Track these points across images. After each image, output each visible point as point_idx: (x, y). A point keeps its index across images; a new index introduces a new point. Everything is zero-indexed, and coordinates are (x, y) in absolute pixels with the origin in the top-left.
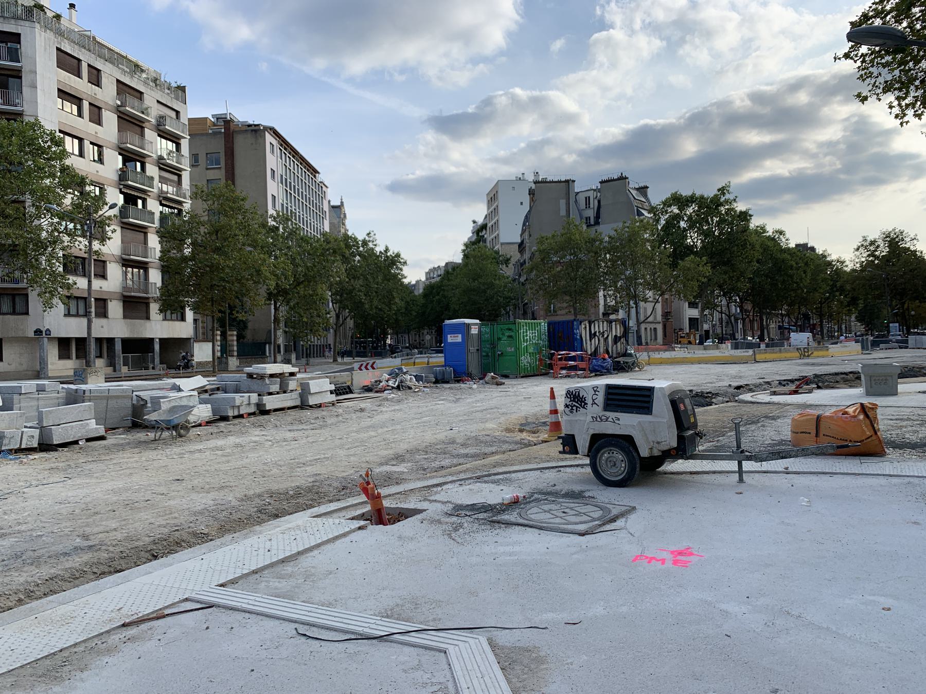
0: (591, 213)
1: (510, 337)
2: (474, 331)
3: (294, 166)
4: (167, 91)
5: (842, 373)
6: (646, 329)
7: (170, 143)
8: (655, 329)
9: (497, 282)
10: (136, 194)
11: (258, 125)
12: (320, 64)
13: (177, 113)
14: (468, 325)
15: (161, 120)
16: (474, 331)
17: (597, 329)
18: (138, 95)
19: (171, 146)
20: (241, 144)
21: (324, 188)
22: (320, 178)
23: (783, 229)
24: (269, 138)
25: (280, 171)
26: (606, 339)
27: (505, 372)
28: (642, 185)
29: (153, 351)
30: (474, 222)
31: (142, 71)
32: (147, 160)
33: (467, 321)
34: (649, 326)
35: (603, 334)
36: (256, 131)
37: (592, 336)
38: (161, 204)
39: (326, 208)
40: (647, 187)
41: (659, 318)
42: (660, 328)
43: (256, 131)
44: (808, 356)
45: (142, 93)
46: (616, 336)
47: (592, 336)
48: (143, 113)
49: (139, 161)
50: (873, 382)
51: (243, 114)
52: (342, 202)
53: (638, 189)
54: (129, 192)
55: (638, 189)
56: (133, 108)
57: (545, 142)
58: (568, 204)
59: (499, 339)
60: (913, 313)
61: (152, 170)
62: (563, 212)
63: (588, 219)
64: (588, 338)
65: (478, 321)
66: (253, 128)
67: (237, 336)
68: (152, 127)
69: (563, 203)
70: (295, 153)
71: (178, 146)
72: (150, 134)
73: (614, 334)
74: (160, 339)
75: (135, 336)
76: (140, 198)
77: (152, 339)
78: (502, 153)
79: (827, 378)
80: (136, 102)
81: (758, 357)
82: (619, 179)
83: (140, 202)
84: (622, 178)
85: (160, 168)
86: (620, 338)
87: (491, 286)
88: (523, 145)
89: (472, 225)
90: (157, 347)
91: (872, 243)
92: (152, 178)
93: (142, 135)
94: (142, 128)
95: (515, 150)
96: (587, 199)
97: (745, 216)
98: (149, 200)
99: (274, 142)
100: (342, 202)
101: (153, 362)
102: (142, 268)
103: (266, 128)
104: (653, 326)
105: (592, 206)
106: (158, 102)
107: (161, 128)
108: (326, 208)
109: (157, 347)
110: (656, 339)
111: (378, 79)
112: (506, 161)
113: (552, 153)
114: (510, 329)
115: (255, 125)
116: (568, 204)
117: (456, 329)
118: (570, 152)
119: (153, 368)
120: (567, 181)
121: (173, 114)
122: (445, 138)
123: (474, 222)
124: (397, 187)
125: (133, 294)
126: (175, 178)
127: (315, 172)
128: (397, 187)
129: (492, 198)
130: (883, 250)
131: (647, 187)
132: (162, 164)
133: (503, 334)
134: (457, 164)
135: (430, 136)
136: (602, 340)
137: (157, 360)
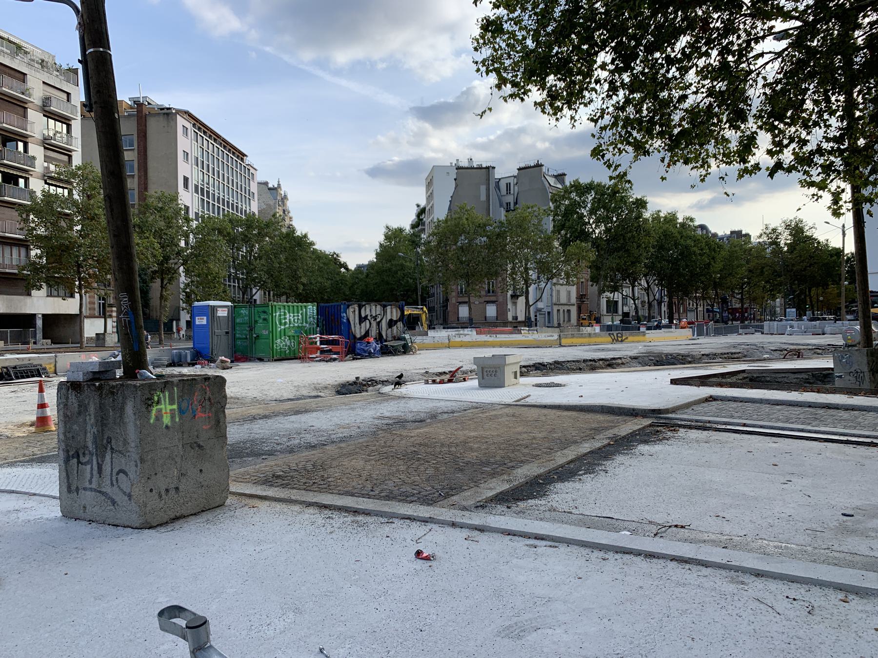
0: (510, 199)
1: (265, 319)
2: (222, 313)
3: (211, 147)
4: (55, 73)
5: (590, 360)
6: (558, 310)
7: (59, 124)
8: (569, 311)
9: (408, 264)
10: (18, 173)
11: (170, 109)
12: (307, 55)
13: (68, 94)
14: (214, 309)
15: (47, 101)
16: (222, 313)
17: (368, 312)
18: (22, 76)
19: (62, 128)
20: (153, 126)
21: (252, 171)
22: (247, 160)
23: (693, 217)
24: (181, 121)
25: (195, 152)
26: (379, 323)
27: (260, 355)
28: (560, 172)
29: (34, 326)
30: (418, 206)
31: (26, 53)
32: (29, 140)
33: (212, 303)
34: (561, 308)
35: (375, 318)
36: (168, 114)
37: (362, 320)
38: (46, 183)
39: (254, 188)
40: (565, 175)
41: (574, 300)
42: (574, 310)
43: (168, 114)
44: (622, 341)
45: (25, 74)
46: (391, 320)
47: (362, 320)
48: (23, 94)
49: (21, 141)
50: (485, 374)
51: (160, 99)
52: (279, 185)
53: (556, 177)
54: (6, 170)
55: (556, 177)
56: (11, 89)
57: (522, 131)
58: (488, 190)
59: (256, 322)
60: (821, 298)
61: (36, 150)
62: (483, 198)
63: (508, 204)
64: (357, 321)
65: (229, 304)
66: (165, 111)
67: (117, 312)
68: (36, 108)
69: (483, 188)
70: (215, 137)
71: (69, 127)
72: (34, 116)
73: (389, 318)
74: (43, 315)
75: (12, 312)
76: (22, 177)
77: (34, 315)
78: (480, 140)
79: (568, 365)
80: (15, 83)
81: (564, 341)
82: (534, 166)
83: (21, 182)
84: (539, 166)
85: (45, 148)
86: (396, 322)
87: (402, 267)
88: (499, 132)
89: (416, 208)
90: (39, 323)
91: (774, 230)
92: (34, 158)
93: (25, 116)
94: (26, 108)
95: (492, 137)
96: (508, 186)
97: (641, 204)
98: (31, 179)
99: (189, 125)
100: (279, 185)
101: (35, 337)
102: (23, 246)
103: (179, 112)
104: (566, 308)
105: (512, 192)
106: (44, 83)
107: (47, 109)
108: (254, 188)
109: (39, 323)
110: (569, 320)
111: (361, 70)
112: (483, 147)
113: (527, 140)
114: (264, 312)
115: (168, 109)
116: (488, 190)
117: (203, 311)
118: (544, 139)
119: (35, 343)
120: (488, 168)
121: (65, 96)
122: (427, 126)
123: (418, 206)
124: (377, 172)
125: (7, 271)
126: (66, 158)
127: (241, 155)
128: (377, 172)
129: (429, 184)
130: (785, 239)
131: (565, 175)
132: (47, 144)
133: (259, 317)
134: (435, 150)
135: (413, 124)
136: (374, 324)
137: (39, 335)
